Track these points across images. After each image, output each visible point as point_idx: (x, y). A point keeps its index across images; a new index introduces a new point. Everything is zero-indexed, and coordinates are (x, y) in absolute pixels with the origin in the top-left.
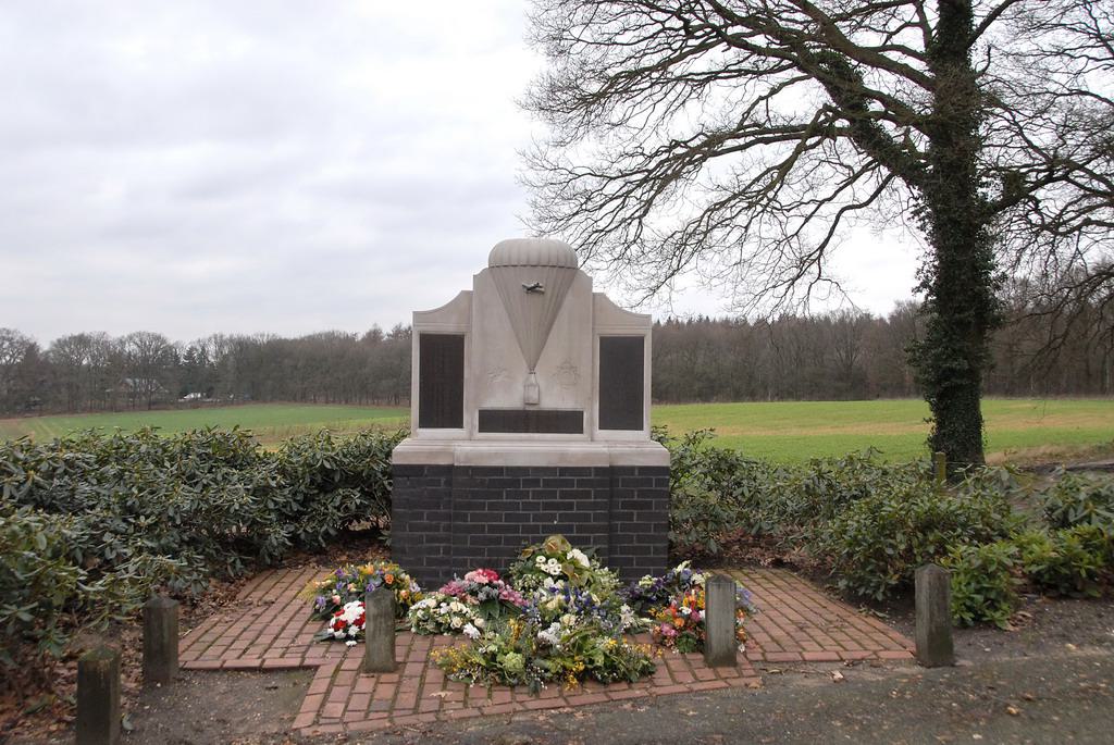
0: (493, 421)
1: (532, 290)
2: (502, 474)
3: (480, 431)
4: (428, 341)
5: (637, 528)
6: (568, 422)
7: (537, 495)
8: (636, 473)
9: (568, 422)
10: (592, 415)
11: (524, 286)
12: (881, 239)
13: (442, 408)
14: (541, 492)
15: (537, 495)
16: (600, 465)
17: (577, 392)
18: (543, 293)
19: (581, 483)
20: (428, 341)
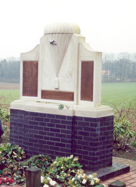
0: (46, 94)
1: (51, 43)
2: (82, 120)
3: (81, 100)
4: (25, 63)
5: (83, 143)
6: (69, 96)
7: (49, 125)
8: (84, 119)
9: (69, 96)
10: (77, 95)
11: (50, 42)
12: (2, 72)
13: (30, 89)
14: (50, 124)
15: (49, 125)
16: (32, 111)
17: (71, 84)
18: (56, 44)
19: (63, 122)
20: (25, 63)
